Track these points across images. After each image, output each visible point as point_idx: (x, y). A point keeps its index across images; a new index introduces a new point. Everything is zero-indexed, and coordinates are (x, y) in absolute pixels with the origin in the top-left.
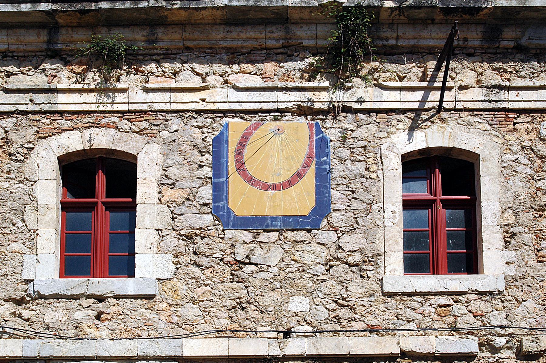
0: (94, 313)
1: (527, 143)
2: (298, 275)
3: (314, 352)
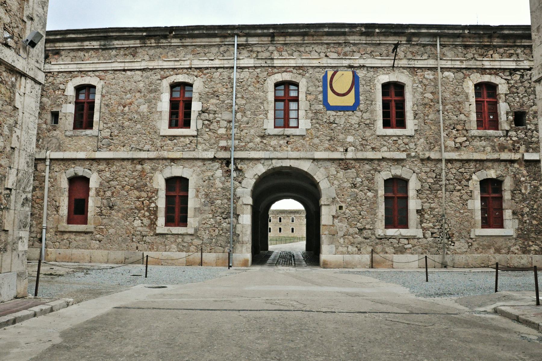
0: (286, 141)
1: (421, 80)
2: (350, 128)
3: (355, 157)
